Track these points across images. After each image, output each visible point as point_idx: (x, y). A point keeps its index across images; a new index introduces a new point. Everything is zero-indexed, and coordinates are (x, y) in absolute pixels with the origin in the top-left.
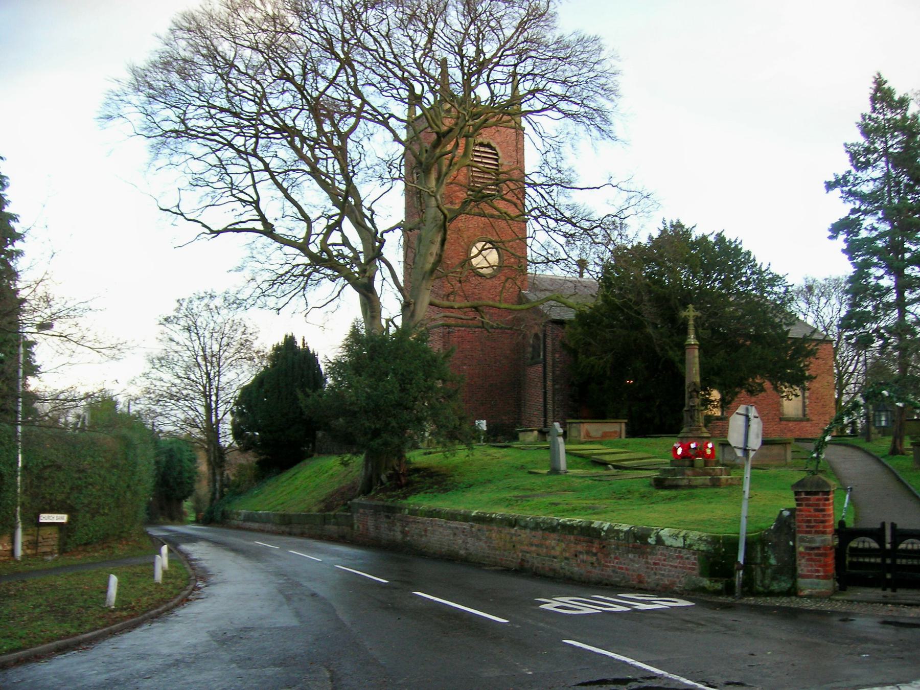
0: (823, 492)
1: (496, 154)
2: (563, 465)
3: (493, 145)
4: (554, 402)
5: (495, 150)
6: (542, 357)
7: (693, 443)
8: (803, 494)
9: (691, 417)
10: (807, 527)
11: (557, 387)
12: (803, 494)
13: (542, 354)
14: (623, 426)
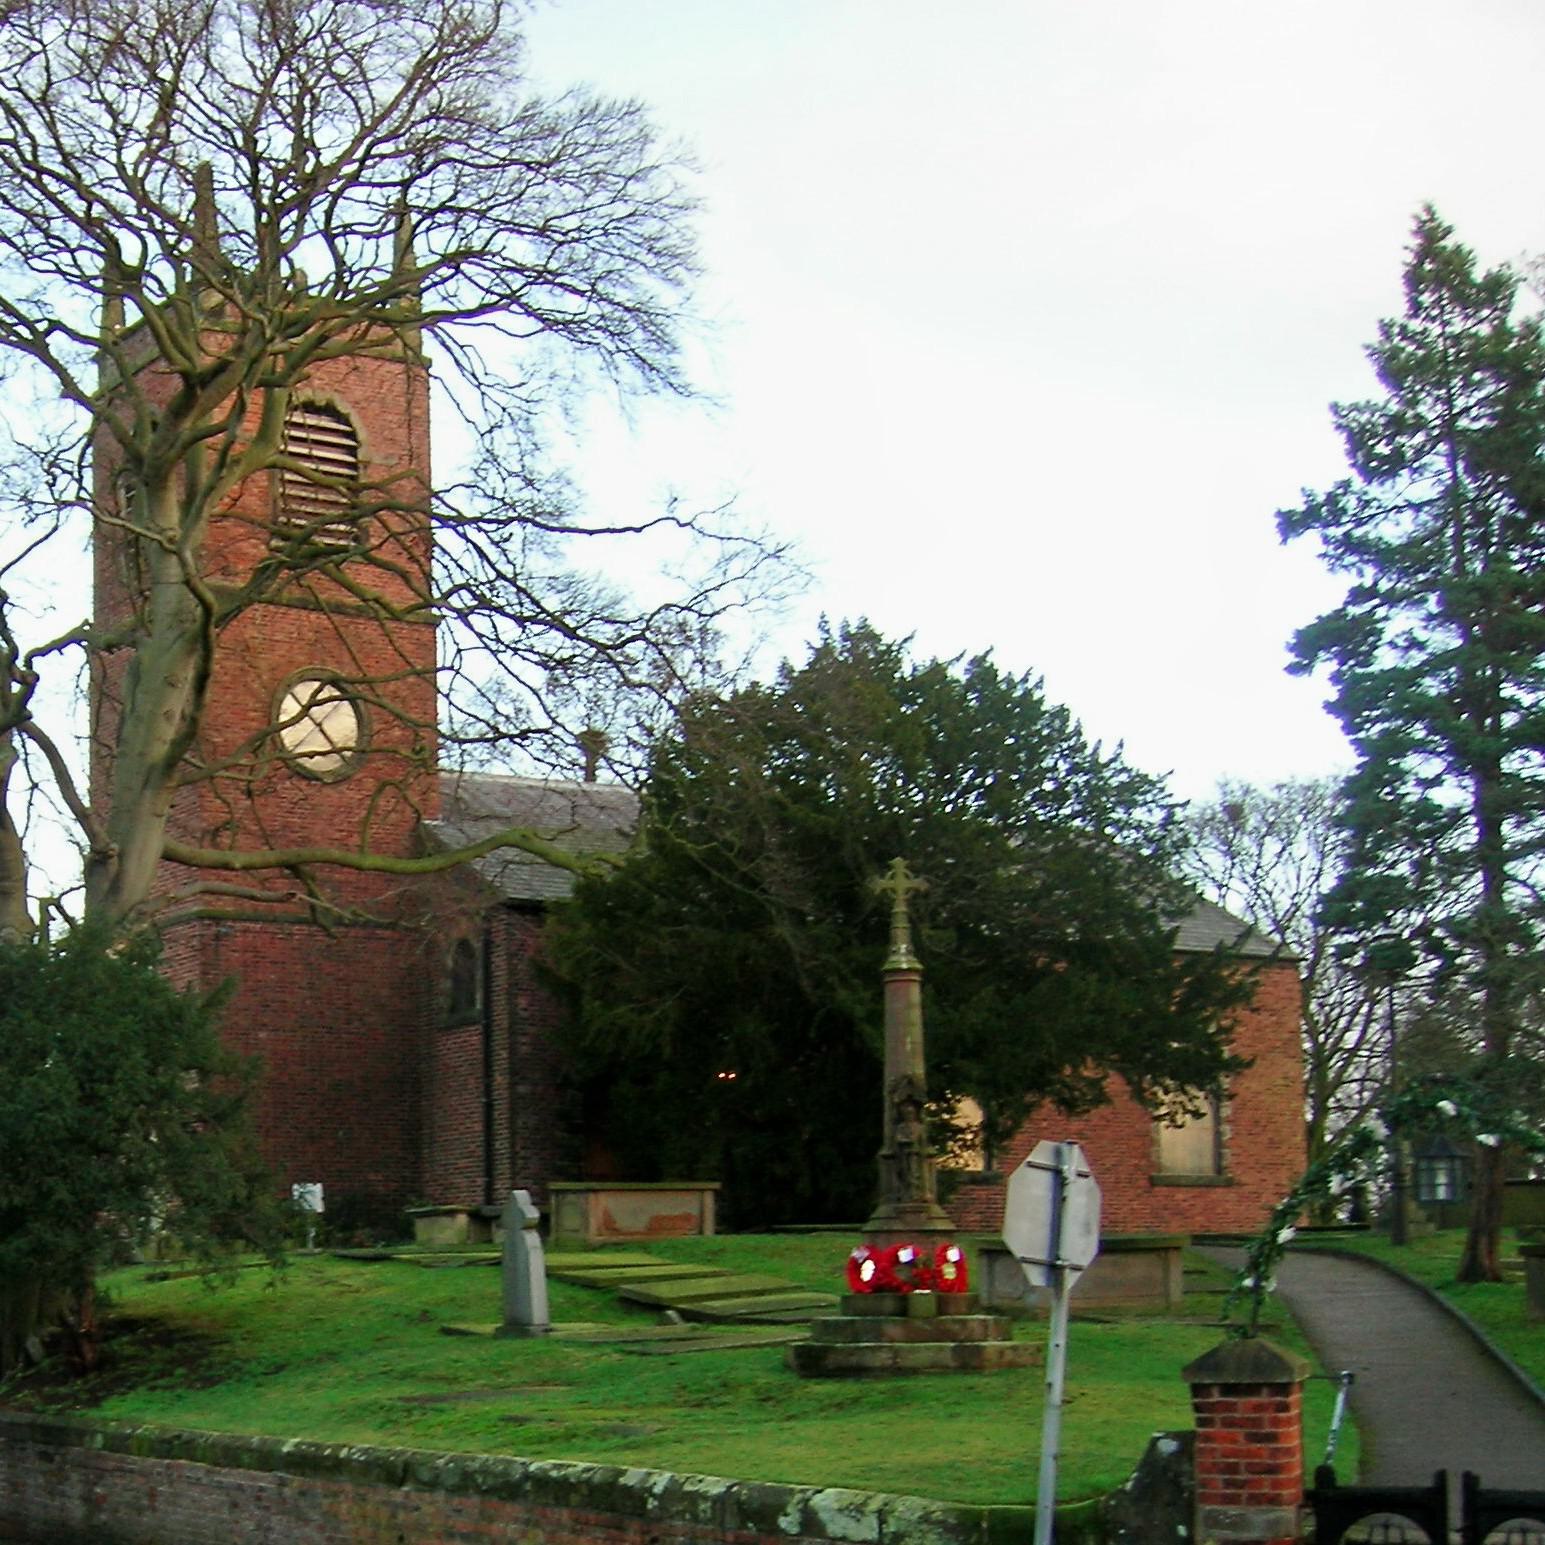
0: (1270, 1385)
1: (351, 435)
2: (539, 1312)
3: (343, 407)
4: (513, 1133)
5: (347, 423)
6: (479, 1006)
7: (904, 1247)
8: (1215, 1391)
9: (901, 1175)
10: (1228, 1484)
11: (522, 1089)
12: (1215, 1391)
13: (479, 996)
14: (709, 1200)
